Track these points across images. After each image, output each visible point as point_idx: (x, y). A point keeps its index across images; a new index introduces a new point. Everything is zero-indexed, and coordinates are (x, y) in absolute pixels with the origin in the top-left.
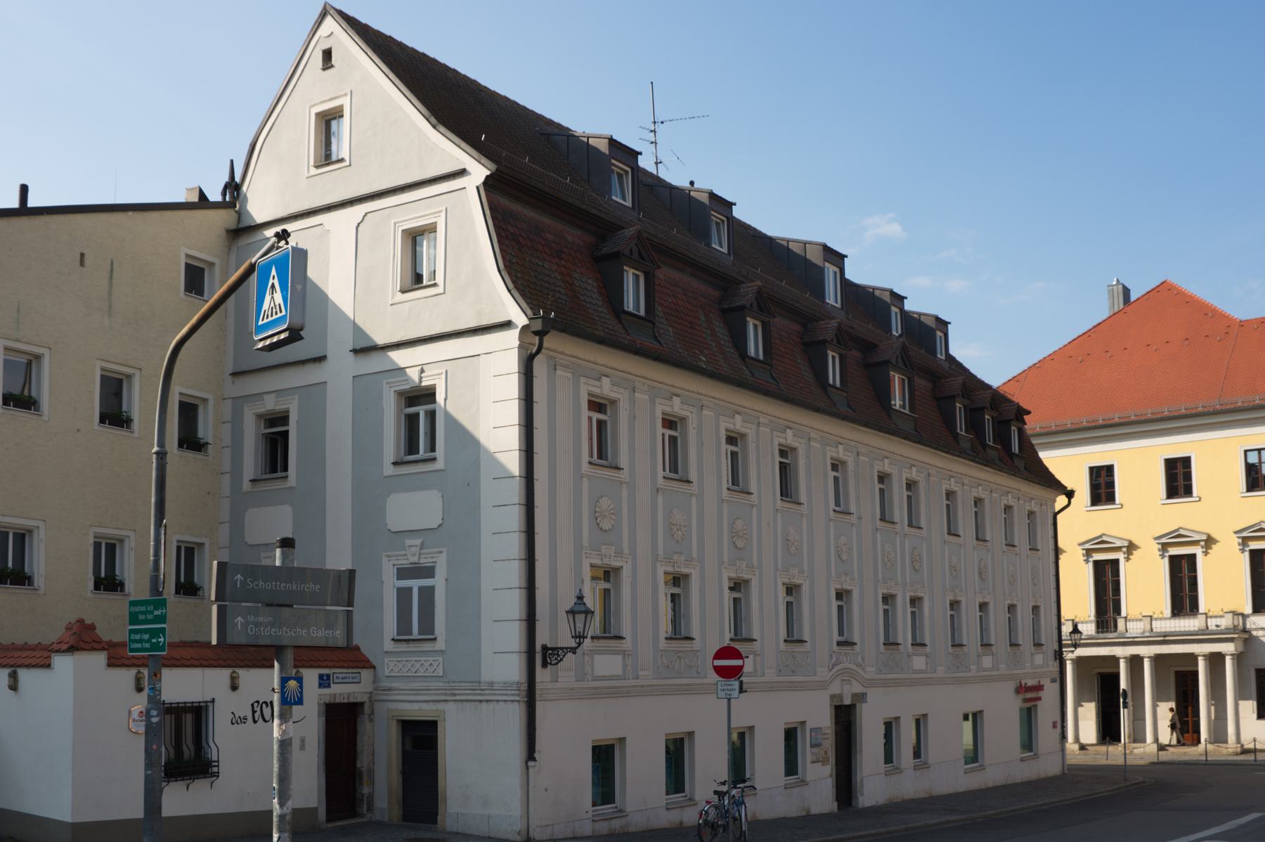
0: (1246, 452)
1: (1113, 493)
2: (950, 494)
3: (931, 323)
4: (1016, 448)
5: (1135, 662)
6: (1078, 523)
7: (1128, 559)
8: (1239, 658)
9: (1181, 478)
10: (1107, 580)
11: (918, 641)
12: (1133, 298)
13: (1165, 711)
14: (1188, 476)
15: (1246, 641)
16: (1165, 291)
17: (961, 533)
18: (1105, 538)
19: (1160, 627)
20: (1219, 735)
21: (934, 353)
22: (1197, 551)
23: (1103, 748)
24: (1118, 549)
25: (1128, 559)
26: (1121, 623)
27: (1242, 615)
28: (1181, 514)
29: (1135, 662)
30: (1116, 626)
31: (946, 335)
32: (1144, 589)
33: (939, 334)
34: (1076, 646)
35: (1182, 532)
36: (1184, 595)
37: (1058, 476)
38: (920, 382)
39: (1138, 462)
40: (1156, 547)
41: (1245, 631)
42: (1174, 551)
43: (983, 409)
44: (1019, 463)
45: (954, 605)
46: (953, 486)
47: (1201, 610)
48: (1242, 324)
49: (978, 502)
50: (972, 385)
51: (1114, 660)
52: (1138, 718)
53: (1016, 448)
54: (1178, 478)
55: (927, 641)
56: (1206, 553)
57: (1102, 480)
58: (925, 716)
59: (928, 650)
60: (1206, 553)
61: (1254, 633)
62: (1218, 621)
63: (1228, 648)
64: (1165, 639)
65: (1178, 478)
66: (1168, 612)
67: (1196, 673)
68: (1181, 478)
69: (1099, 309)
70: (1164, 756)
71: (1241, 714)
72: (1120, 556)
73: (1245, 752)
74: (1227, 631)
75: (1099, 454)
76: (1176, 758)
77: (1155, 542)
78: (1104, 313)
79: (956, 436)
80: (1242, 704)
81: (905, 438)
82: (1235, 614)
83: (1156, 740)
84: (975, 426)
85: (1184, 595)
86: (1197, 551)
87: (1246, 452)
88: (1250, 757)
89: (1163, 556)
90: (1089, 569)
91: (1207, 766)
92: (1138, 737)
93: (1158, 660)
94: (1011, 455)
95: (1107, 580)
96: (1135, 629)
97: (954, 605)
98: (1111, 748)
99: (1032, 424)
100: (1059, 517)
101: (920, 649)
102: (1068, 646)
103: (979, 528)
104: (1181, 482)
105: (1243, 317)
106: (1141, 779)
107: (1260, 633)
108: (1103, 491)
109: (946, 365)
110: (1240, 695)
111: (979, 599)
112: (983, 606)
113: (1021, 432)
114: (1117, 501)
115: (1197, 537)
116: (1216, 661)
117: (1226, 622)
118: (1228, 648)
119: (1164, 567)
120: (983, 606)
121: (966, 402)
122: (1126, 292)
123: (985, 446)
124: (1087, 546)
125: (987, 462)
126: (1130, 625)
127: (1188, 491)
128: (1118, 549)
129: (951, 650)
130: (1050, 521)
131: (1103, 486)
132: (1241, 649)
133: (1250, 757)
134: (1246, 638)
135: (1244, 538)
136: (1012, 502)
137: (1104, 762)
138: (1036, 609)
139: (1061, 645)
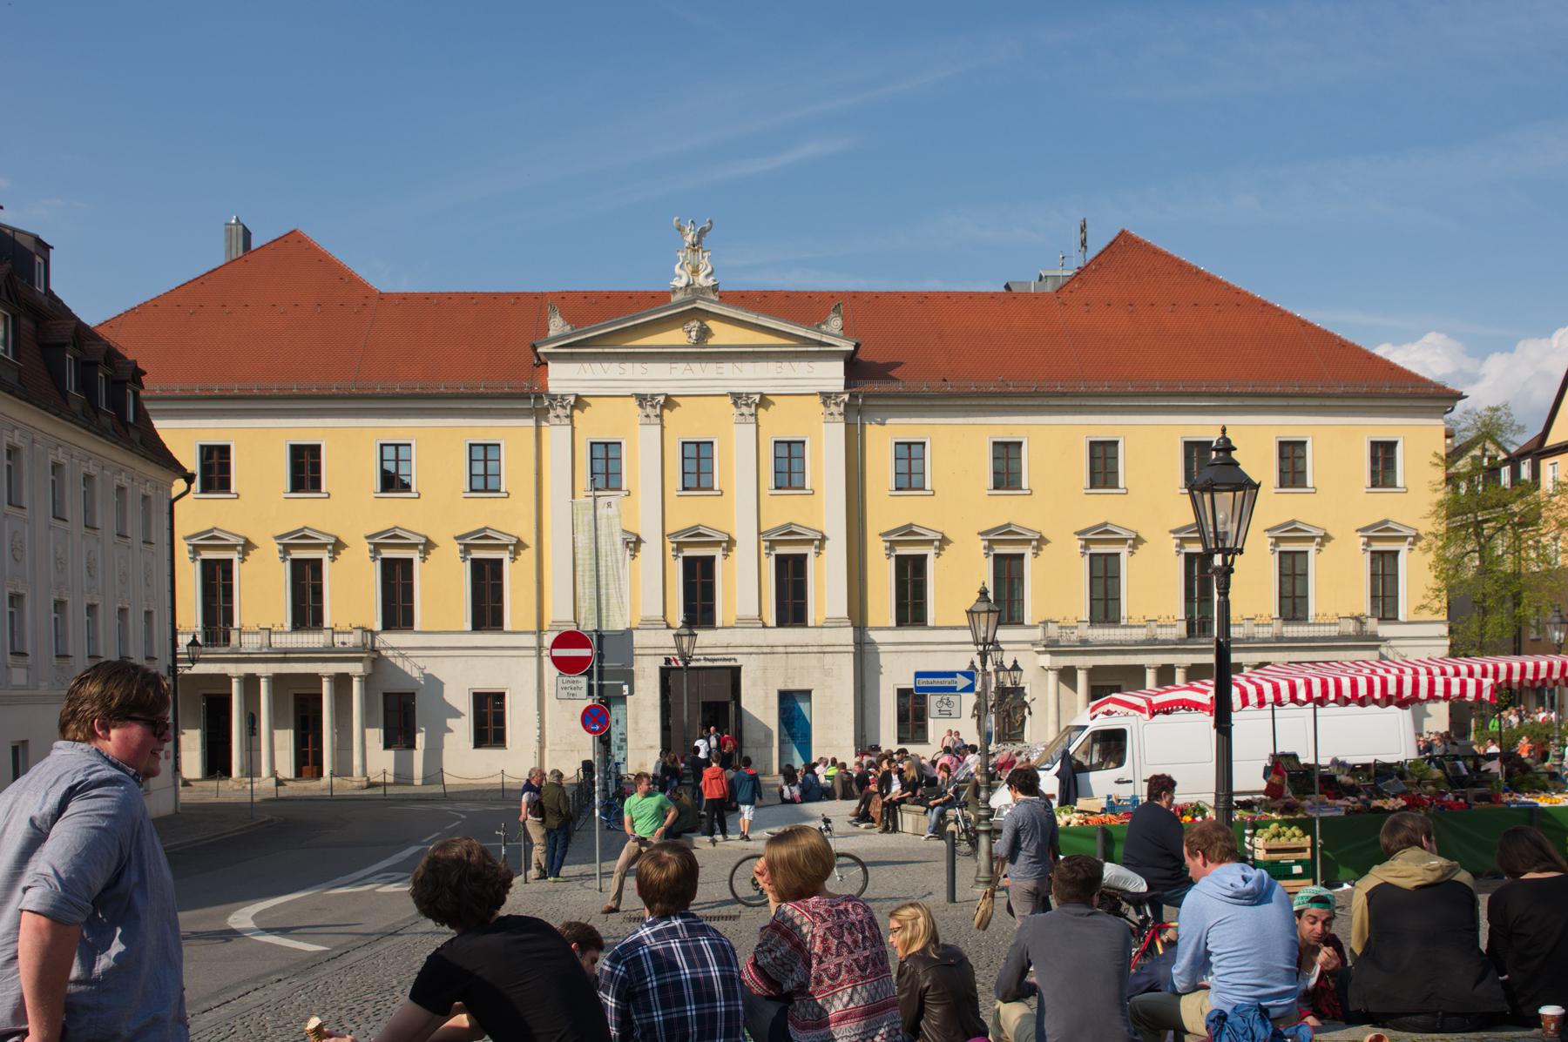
0: (382, 446)
1: (228, 480)
2: (56, 467)
3: (29, 244)
4: (131, 418)
5: (250, 682)
6: (195, 513)
7: (243, 560)
8: (367, 680)
9: (308, 468)
10: (217, 580)
11: (17, 649)
12: (254, 246)
13: (285, 740)
14: (317, 468)
15: (374, 661)
16: (293, 242)
17: (68, 517)
18: (216, 533)
19: (280, 641)
20: (342, 769)
21: (32, 282)
22: (415, 555)
23: (212, 784)
24: (232, 547)
25: (243, 560)
26: (234, 636)
27: (371, 631)
28: (306, 512)
29: (250, 682)
30: (227, 639)
31: (47, 262)
32: (262, 597)
33: (38, 259)
34: (193, 661)
35: (307, 532)
36: (307, 605)
37: (177, 456)
38: (25, 322)
39: (260, 445)
40: (276, 548)
41: (373, 650)
42: (689, 552)
43: (96, 364)
44: (135, 435)
45: (60, 605)
46: (61, 457)
47: (327, 623)
48: (382, 297)
49: (88, 478)
50: (82, 333)
51: (225, 679)
52: (251, 749)
53: (131, 418)
54: (305, 469)
55: (28, 650)
56: (333, 559)
57: (215, 460)
58: (25, 742)
59: (29, 660)
60: (333, 559)
61: (383, 653)
62: (345, 638)
63: (355, 669)
64: (286, 656)
65: (305, 469)
66: (288, 626)
67: (319, 698)
68: (308, 468)
69: (213, 254)
70: (283, 792)
71: (368, 744)
72: (235, 556)
73: (371, 785)
74: (355, 649)
75: (214, 430)
76: (297, 793)
77: (275, 542)
78: (220, 260)
79: (64, 395)
80: (278, 734)
81: (10, 393)
82: (364, 630)
83: (273, 773)
84: (86, 385)
85: (307, 605)
86: (505, 556)
87: (382, 446)
88: (380, 791)
89: (284, 559)
90: (377, 568)
91: (333, 801)
92: (251, 770)
93: (276, 680)
94: (126, 425)
95: (217, 580)
96: (251, 643)
97: (60, 605)
98: (222, 783)
99: (151, 385)
100: (177, 504)
101: (20, 660)
102: (183, 661)
103: (89, 511)
104: (308, 474)
105: (384, 290)
106: (268, 817)
107: (390, 653)
108: (215, 475)
109: (45, 301)
110: (367, 723)
111: (87, 601)
112: (91, 608)
113: (136, 394)
114: (233, 489)
115: (324, 540)
116: (342, 683)
117: (353, 640)
118: (355, 669)
119: (284, 573)
120: (91, 608)
121: (78, 353)
122: (247, 235)
123: (96, 409)
124: (195, 541)
125: (101, 432)
126: (245, 638)
127: (316, 485)
128: (232, 547)
129: (55, 661)
130: (166, 509)
131: (216, 469)
132: (369, 671)
133: (380, 791)
134: (376, 660)
135: (376, 545)
136: (125, 482)
137: (213, 799)
138: (148, 614)
139: (175, 660)
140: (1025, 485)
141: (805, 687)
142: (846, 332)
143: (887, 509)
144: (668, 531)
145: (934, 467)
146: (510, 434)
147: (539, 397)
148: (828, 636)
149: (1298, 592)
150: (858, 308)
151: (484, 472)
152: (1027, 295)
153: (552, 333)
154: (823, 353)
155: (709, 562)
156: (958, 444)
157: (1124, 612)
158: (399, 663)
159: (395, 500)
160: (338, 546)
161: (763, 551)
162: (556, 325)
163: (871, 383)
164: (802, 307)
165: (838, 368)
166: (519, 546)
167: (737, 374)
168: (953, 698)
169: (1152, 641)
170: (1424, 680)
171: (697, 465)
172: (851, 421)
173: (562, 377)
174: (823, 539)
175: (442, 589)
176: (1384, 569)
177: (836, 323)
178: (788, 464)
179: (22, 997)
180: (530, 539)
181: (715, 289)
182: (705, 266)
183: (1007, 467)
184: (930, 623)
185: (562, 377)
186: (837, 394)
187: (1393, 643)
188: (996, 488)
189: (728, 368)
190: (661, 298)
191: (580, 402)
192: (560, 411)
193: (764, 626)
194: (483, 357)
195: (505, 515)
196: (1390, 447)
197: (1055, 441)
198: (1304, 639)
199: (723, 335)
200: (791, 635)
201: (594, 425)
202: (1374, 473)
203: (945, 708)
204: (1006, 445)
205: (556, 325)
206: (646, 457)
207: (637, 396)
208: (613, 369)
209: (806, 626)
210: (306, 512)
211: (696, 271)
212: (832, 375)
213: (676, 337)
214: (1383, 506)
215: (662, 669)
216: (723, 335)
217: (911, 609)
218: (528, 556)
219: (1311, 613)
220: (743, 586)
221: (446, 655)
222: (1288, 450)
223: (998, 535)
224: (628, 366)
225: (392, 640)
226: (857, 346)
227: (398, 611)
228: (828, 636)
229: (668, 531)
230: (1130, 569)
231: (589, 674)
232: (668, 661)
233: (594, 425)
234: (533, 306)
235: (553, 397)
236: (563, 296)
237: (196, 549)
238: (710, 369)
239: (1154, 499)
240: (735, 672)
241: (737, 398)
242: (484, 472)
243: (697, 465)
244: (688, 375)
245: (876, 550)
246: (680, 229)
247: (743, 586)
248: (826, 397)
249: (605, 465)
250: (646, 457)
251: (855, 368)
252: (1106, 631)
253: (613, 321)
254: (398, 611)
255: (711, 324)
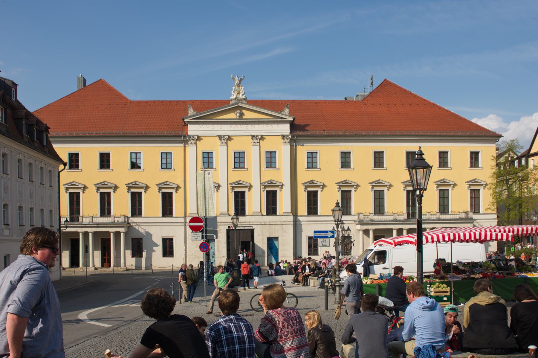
0: (131, 153)
1: (78, 165)
2: (19, 161)
3: (10, 84)
4: (45, 144)
5: (86, 234)
6: (67, 176)
7: (83, 192)
8: (126, 234)
9: (106, 161)
10: (75, 199)
11: (6, 223)
12: (87, 84)
13: (98, 254)
14: (109, 161)
15: (128, 227)
16: (101, 83)
17: (23, 178)
18: (74, 183)
19: (96, 220)
20: (118, 264)
21: (11, 97)
22: (142, 191)
23: (73, 269)
24: (80, 188)
25: (83, 192)
26: (80, 219)
27: (127, 217)
28: (105, 176)
29: (86, 234)
30: (78, 220)
31: (16, 90)
32: (90, 205)
33: (13, 89)
34: (66, 227)
35: (105, 183)
36: (105, 208)
37: (61, 157)
38: (9, 111)
39: (89, 153)
40: (95, 188)
41: (128, 223)
42: (236, 190)
43: (33, 125)
44: (46, 150)
45: (20, 208)
46: (21, 157)
47: (112, 214)
48: (131, 102)
49: (30, 164)
50: (28, 114)
51: (77, 233)
52: (86, 257)
53: (45, 144)
54: (105, 161)
55: (10, 223)
56: (114, 192)
57: (74, 158)
58: (8, 255)
59: (10, 227)
60: (114, 192)
61: (132, 224)
62: (118, 219)
63: (122, 230)
64: (98, 225)
65: (105, 161)
66: (99, 215)
67: (110, 240)
68: (106, 161)
69: (73, 87)
70: (97, 272)
71: (126, 255)
72: (80, 191)
73: (127, 270)
74: (122, 223)
75: (73, 148)
76: (102, 273)
77: (94, 186)
78: (75, 89)
79: (22, 136)
80: (96, 252)
81: (4, 135)
82: (125, 216)
83: (94, 266)
84: (30, 132)
85: (105, 208)
86: (173, 191)
87: (131, 153)
88: (130, 272)
89: (97, 192)
90: (129, 195)
91: (114, 275)
92: (86, 265)
93: (95, 234)
94: (43, 146)
95: (75, 199)
96: (86, 221)
97: (20, 208)
98: (76, 269)
99: (52, 132)
100: (61, 173)
101: (7, 227)
102: (63, 227)
103: (30, 176)
104: (106, 163)
105: (132, 100)
106: (92, 281)
107: (134, 224)
108: (74, 163)
109: (16, 103)
110: (126, 248)
111: (30, 207)
112: (31, 209)
113: (47, 135)
114: (80, 168)
115: (111, 186)
116: (117, 235)
117: (121, 220)
118: (122, 230)
119: (98, 197)
120: (31, 209)
121: (27, 121)
122: (85, 81)
123: (33, 141)
124: (67, 186)
125: (35, 148)
126: (84, 219)
127: (108, 167)
128: (80, 188)
129: (19, 227)
130: (57, 175)
131: (74, 161)
132: (127, 230)
133: (130, 272)
134: (129, 227)
135: (129, 187)
136: (43, 166)
137: (73, 275)
138: (51, 211)
139: (60, 227)
140: (352, 166)
141: (276, 236)
142: (290, 114)
143: (304, 175)
144: (229, 182)
145: (320, 160)
146: (175, 149)
147: (185, 136)
148: (284, 219)
149: (445, 203)
150: (294, 106)
151: (166, 162)
152: (352, 101)
153: (189, 114)
154: (282, 121)
155: (243, 193)
156: (329, 152)
157: (386, 210)
158: (137, 228)
159: (136, 172)
160: (116, 188)
161: (262, 189)
162: (191, 112)
163: (299, 132)
164: (275, 105)
165: (287, 126)
166: (178, 187)
167: (253, 129)
168: (327, 240)
169: (395, 220)
170: (488, 234)
171: (239, 160)
172: (292, 145)
173: (193, 130)
174: (283, 185)
175: (152, 202)
176: (475, 195)
177: (287, 111)
178: (270, 159)
179: (8, 343)
180: (182, 185)
181: (245, 99)
182: (242, 91)
183: (345, 160)
184: (319, 214)
185: (193, 130)
186: (287, 135)
187: (478, 221)
188: (342, 168)
189: (250, 127)
190: (227, 102)
191: (199, 138)
192: (192, 141)
193: (262, 215)
194: (166, 122)
195: (173, 177)
196: (477, 153)
197: (362, 152)
198: (447, 220)
199: (248, 115)
200: (272, 218)
201: (204, 146)
202: (471, 163)
203: (324, 243)
204: (345, 153)
205: (191, 112)
206: (222, 157)
207: (219, 136)
208: (210, 127)
209: (276, 215)
210: (105, 176)
211: (239, 93)
212: (285, 129)
213: (232, 116)
214: (475, 174)
215: (227, 230)
216: (248, 115)
217: (313, 209)
218: (181, 191)
219: (450, 210)
220: (255, 201)
221: (153, 225)
222: (442, 154)
223: (342, 184)
224: (215, 126)
225: (134, 220)
226: (294, 119)
227: (136, 210)
228: (284, 219)
229: (229, 182)
230: (388, 195)
231: (202, 232)
232: (229, 227)
233: (204, 146)
234: (183, 105)
235: (190, 137)
236: (193, 102)
237: (67, 189)
238: (244, 127)
239: (396, 171)
240: (252, 231)
241: (253, 137)
242: (166, 162)
243: (239, 160)
244: (236, 129)
245: (301, 189)
246: (233, 79)
247: (255, 201)
248: (283, 136)
249: (208, 160)
250: (222, 157)
251: (293, 127)
252: (380, 217)
253: (210, 110)
254: (136, 210)
255: (244, 111)
